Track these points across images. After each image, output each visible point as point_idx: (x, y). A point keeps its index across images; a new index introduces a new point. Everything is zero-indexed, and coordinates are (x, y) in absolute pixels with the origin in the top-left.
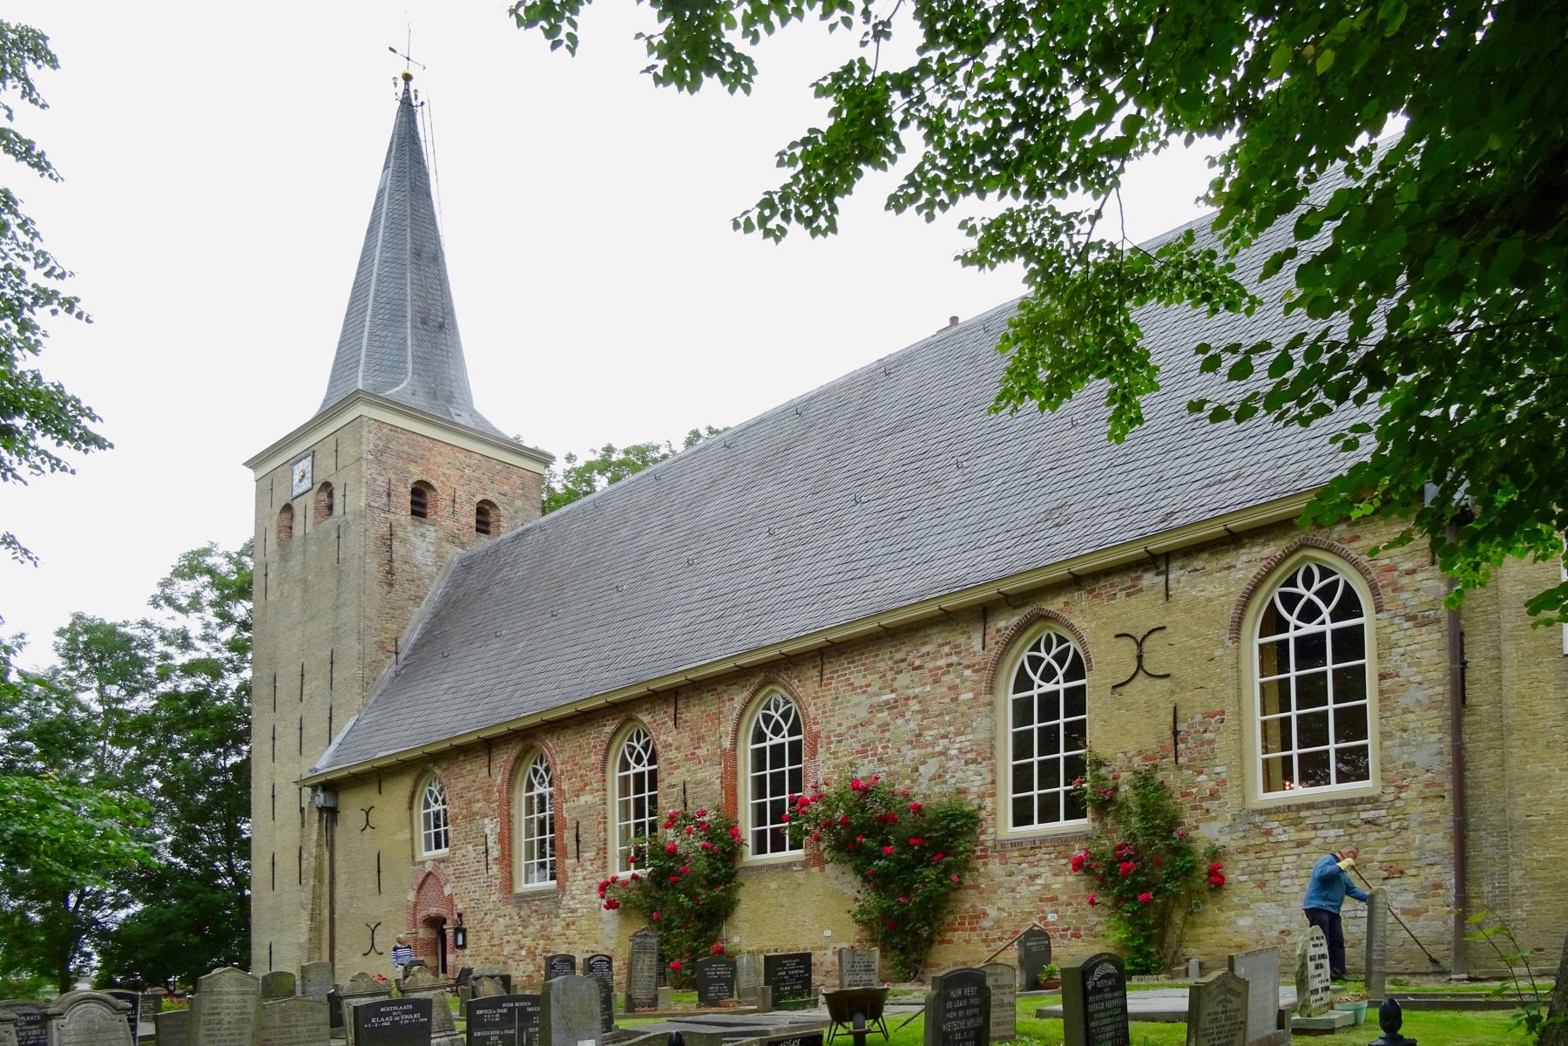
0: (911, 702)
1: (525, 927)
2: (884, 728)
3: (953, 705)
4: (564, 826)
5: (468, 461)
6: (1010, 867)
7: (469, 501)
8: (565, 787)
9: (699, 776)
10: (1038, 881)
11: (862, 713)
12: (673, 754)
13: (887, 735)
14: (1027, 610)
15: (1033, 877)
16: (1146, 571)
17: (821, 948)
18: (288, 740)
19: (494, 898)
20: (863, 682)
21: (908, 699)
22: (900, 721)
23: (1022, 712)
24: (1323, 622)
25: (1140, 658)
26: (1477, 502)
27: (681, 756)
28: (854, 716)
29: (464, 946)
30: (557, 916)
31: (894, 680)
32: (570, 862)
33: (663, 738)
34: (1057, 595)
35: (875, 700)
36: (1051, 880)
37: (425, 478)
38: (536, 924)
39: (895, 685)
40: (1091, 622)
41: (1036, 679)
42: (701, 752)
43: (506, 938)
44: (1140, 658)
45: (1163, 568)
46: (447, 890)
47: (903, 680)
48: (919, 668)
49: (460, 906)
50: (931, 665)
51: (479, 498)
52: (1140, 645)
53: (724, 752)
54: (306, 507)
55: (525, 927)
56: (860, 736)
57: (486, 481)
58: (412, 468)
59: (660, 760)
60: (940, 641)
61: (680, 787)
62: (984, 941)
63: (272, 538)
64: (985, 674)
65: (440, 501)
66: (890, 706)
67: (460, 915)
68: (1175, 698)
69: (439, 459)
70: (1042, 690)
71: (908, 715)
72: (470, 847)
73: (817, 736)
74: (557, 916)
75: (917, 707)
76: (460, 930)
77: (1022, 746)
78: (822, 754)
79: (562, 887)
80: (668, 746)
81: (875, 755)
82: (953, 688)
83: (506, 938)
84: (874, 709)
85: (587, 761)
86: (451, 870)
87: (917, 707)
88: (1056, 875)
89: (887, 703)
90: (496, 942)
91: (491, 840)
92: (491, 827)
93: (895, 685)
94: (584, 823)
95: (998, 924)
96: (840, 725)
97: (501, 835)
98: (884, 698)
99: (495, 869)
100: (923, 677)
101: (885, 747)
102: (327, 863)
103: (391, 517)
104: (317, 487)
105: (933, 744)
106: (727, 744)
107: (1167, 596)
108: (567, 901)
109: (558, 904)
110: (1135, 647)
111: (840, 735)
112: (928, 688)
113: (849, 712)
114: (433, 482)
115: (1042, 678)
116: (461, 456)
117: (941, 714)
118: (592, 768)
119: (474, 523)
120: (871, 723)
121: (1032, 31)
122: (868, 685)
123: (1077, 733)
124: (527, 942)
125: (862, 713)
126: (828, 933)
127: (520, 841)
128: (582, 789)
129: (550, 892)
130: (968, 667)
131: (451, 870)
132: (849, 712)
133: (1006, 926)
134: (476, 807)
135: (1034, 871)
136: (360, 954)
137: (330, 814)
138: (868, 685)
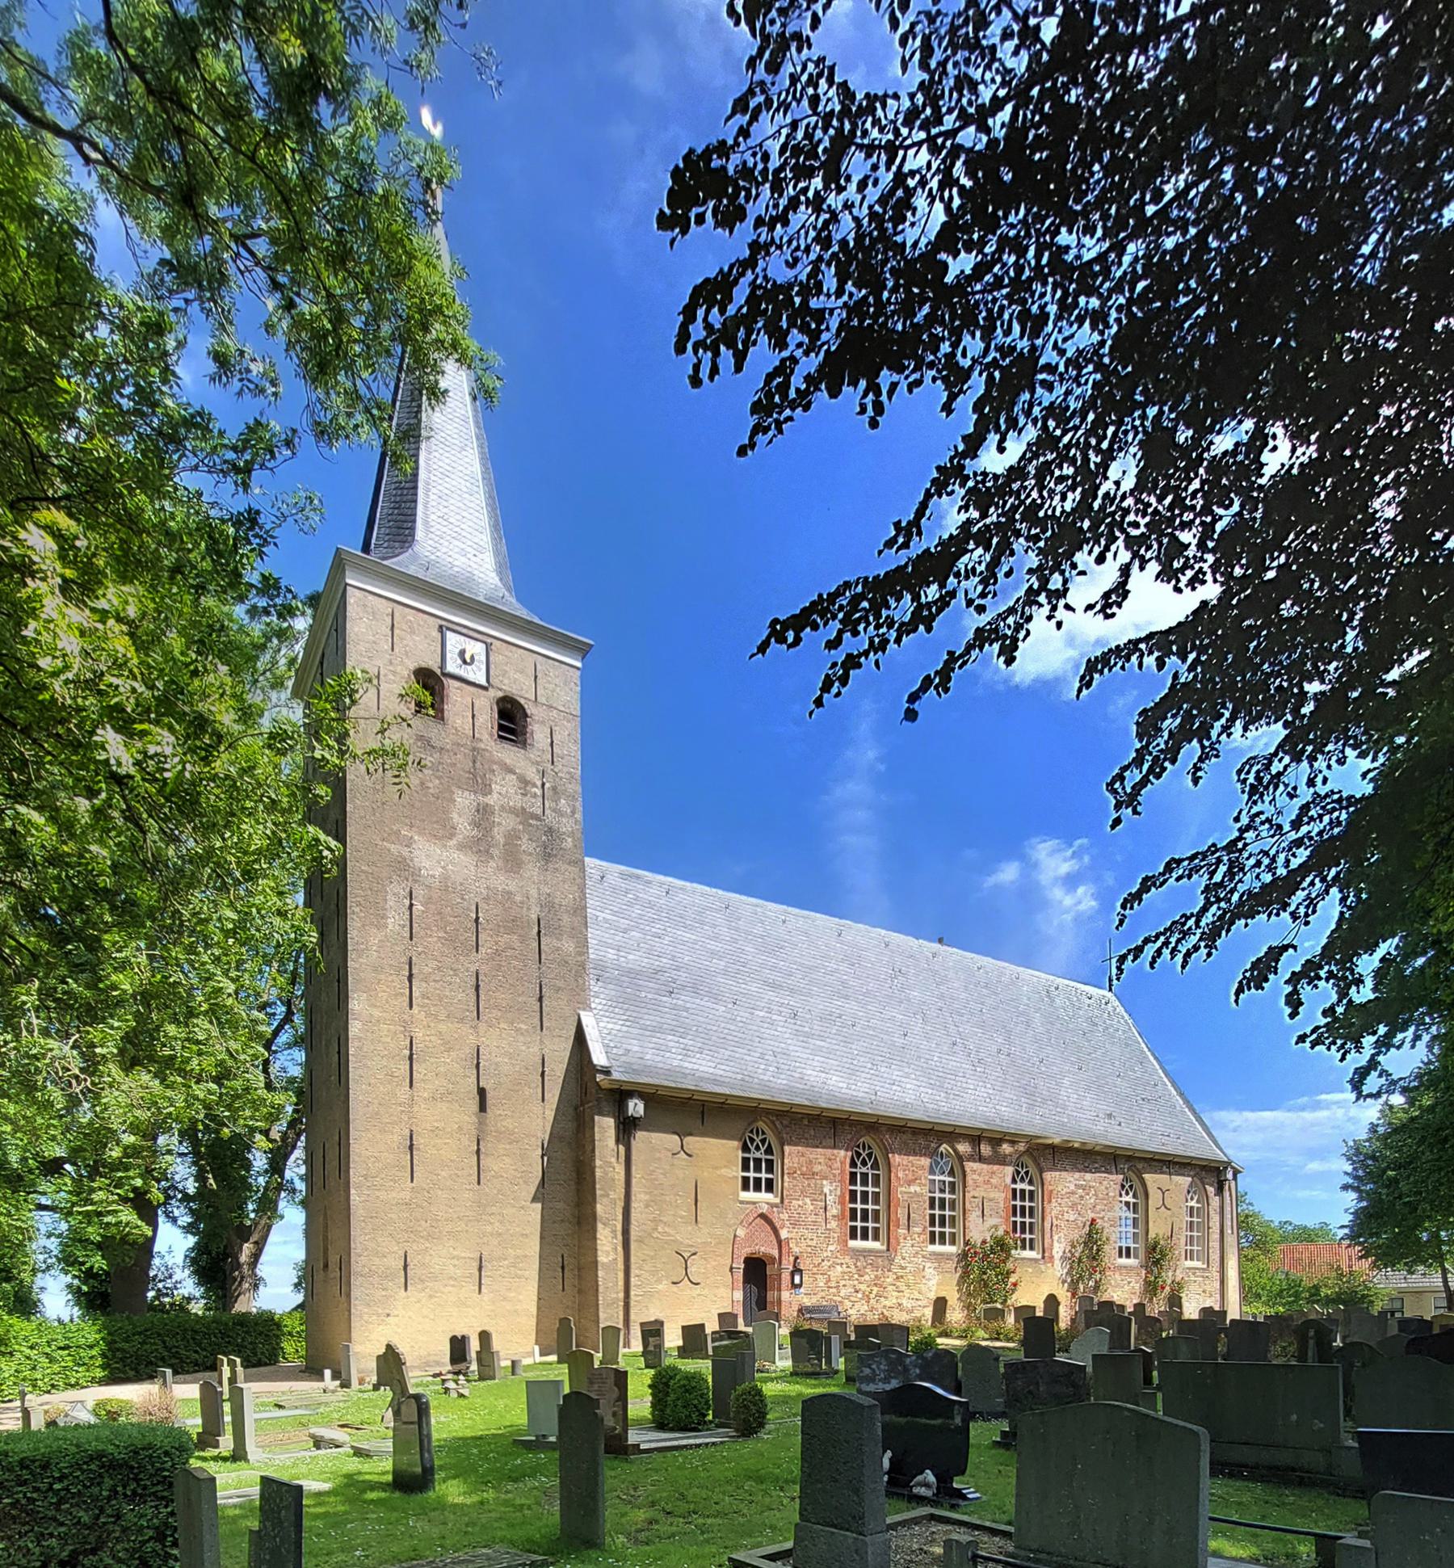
19: (831, 1248)
26: (1061, 902)
29: (800, 1286)
32: (902, 1231)
38: (870, 1275)
76: (797, 1270)
86: (785, 1216)
121: (1201, 471)
124: (863, 1287)
125: (1072, 1187)
134: (817, 1168)
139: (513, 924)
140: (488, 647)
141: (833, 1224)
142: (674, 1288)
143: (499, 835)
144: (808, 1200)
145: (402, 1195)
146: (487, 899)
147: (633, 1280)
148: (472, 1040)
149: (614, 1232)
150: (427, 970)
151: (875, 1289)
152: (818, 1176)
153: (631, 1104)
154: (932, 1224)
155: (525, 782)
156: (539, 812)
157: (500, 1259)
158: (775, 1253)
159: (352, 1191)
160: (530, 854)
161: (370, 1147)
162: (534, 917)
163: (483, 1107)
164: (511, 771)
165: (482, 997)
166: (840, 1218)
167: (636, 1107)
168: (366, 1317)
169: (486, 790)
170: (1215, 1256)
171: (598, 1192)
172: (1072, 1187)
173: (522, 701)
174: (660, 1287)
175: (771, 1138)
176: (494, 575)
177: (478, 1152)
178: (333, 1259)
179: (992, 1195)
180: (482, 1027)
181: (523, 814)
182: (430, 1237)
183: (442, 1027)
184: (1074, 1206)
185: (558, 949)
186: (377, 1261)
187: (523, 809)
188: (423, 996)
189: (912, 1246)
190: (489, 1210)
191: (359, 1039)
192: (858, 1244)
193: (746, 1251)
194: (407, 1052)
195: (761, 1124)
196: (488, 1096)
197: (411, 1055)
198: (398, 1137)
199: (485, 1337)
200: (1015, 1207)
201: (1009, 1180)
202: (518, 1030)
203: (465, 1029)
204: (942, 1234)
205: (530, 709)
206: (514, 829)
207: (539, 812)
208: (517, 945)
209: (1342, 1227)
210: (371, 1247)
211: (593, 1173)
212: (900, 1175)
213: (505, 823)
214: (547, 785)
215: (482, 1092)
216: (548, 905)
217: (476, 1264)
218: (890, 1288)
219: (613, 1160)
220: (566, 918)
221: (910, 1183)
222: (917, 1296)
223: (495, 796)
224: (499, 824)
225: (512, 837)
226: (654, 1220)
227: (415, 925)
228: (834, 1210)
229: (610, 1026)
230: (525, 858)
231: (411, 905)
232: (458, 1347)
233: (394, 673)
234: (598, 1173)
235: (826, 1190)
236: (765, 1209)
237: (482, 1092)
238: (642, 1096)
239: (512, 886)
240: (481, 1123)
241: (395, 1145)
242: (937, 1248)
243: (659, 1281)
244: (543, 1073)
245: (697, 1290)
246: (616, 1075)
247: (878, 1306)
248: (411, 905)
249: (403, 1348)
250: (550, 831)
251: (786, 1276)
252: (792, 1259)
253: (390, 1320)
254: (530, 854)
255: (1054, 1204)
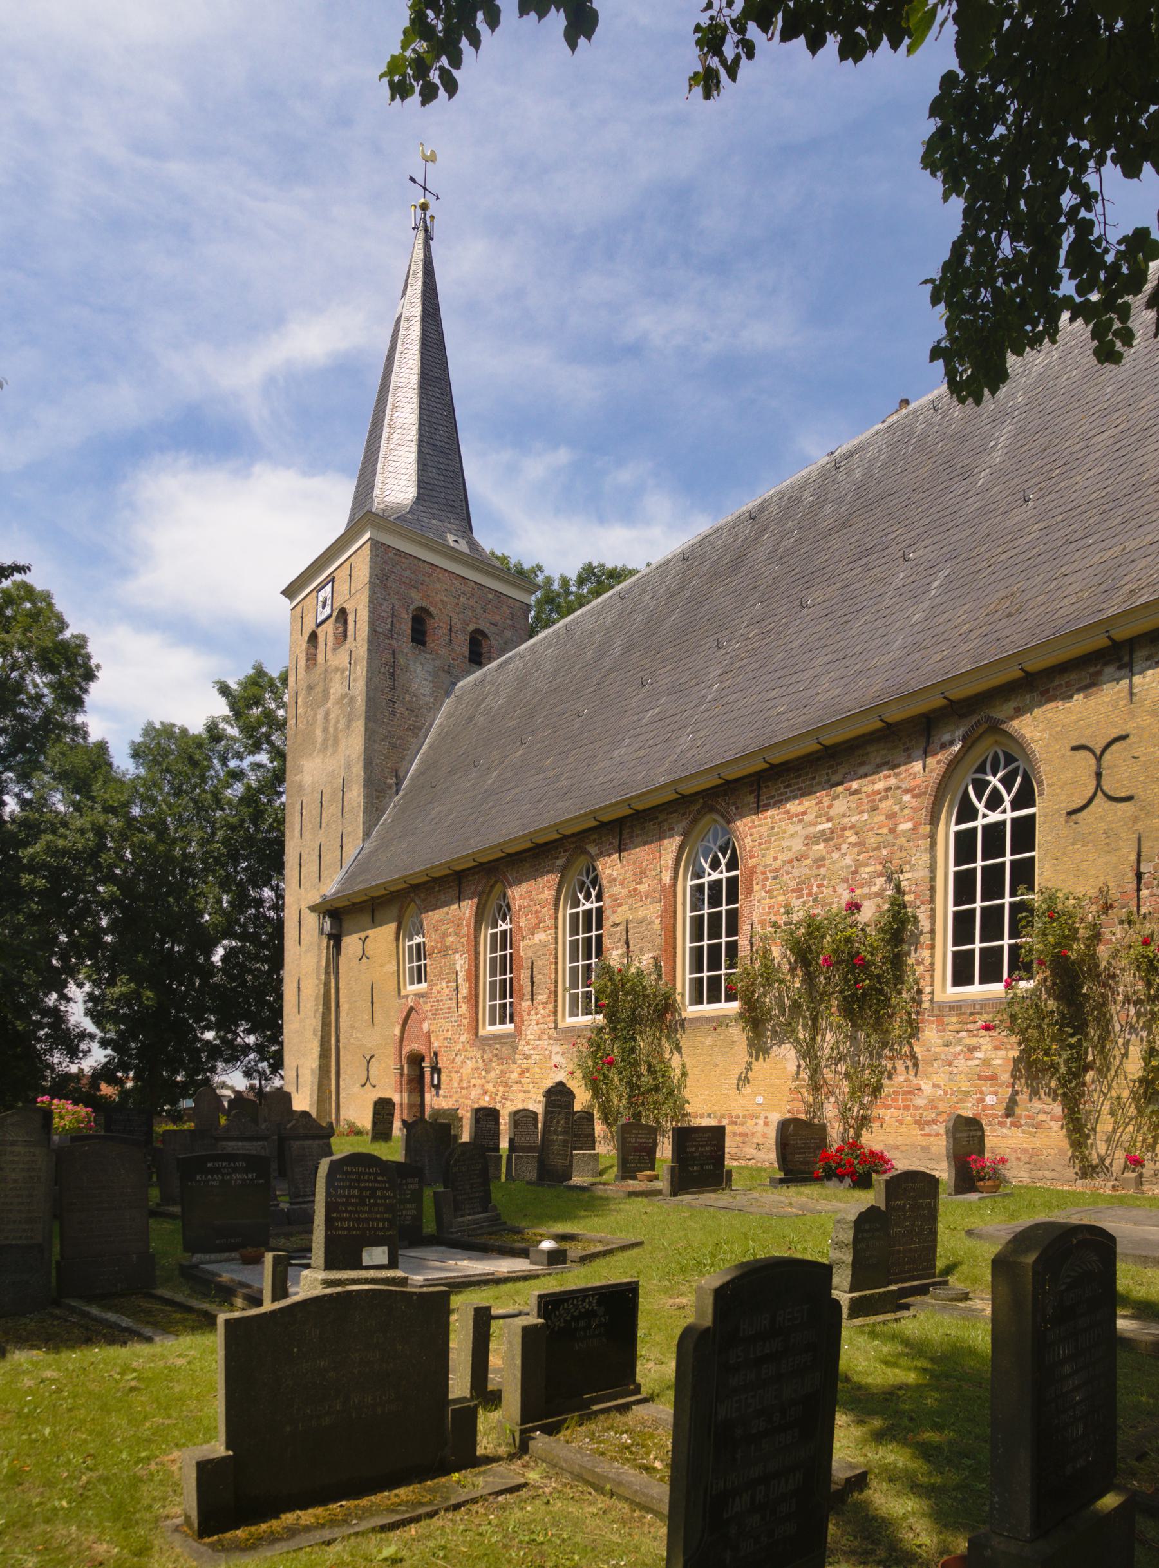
0: (848, 833)
1: (488, 1072)
2: (820, 862)
3: (891, 837)
4: (521, 966)
5: (463, 588)
6: (948, 1035)
7: (464, 630)
8: (522, 924)
9: (641, 914)
10: (978, 1055)
11: (797, 845)
12: (617, 890)
13: (823, 871)
14: (974, 719)
15: (972, 1049)
16: (1106, 664)
17: (753, 1117)
18: (310, 868)
19: (463, 1038)
20: (800, 809)
21: (844, 829)
22: (836, 855)
23: (965, 847)
24: (1004, 811)
25: (1099, 775)
27: (624, 891)
28: (789, 849)
30: (514, 1062)
31: (830, 806)
32: (526, 1004)
33: (608, 871)
34: (1007, 700)
35: (811, 829)
36: (991, 1054)
37: (424, 604)
39: (832, 813)
40: (1040, 729)
41: (981, 807)
42: (643, 888)
43: (473, 1081)
44: (1099, 775)
45: (1126, 659)
46: (425, 1027)
47: (840, 806)
48: (857, 792)
49: (436, 1045)
50: (868, 789)
51: (471, 628)
52: (1099, 759)
53: (664, 887)
54: (328, 632)
55: (488, 1072)
56: (796, 873)
57: (479, 611)
58: (414, 594)
59: (606, 896)
60: (879, 760)
61: (623, 927)
62: (917, 1122)
63: (302, 663)
64: (927, 801)
65: (437, 628)
66: (825, 837)
67: (436, 1054)
68: (1140, 826)
69: (438, 586)
70: (987, 821)
71: (844, 847)
72: (444, 984)
73: (752, 871)
74: (514, 1062)
75: (853, 839)
76: (436, 1069)
77: (964, 887)
78: (758, 893)
79: (518, 1030)
80: (612, 881)
81: (809, 894)
82: (892, 816)
83: (473, 1081)
84: (810, 841)
85: (541, 896)
86: (428, 1007)
87: (853, 839)
88: (996, 1048)
89: (823, 832)
90: (465, 1084)
91: (461, 976)
92: (461, 963)
93: (832, 813)
94: (538, 963)
95: (933, 1102)
96: (775, 859)
97: (468, 971)
98: (820, 827)
99: (464, 1008)
100: (860, 802)
101: (820, 886)
102: (333, 991)
103: (394, 642)
104: (335, 613)
105: (870, 883)
106: (667, 878)
107: (1131, 694)
108: (522, 1047)
109: (515, 1048)
110: (1093, 761)
111: (776, 870)
112: (865, 816)
113: (785, 844)
114: (432, 609)
115: (987, 806)
116: (457, 583)
117: (878, 848)
118: (544, 904)
119: (467, 654)
120: (806, 857)
122: (804, 813)
123: (1024, 873)
125: (797, 845)
126: (760, 1100)
127: (485, 979)
128: (537, 926)
129: (509, 1036)
130: (907, 791)
131: (428, 1007)
132: (785, 844)
133: (942, 1106)
135: (973, 1041)
136: (358, 1085)
137: (336, 939)
138: (804, 813)
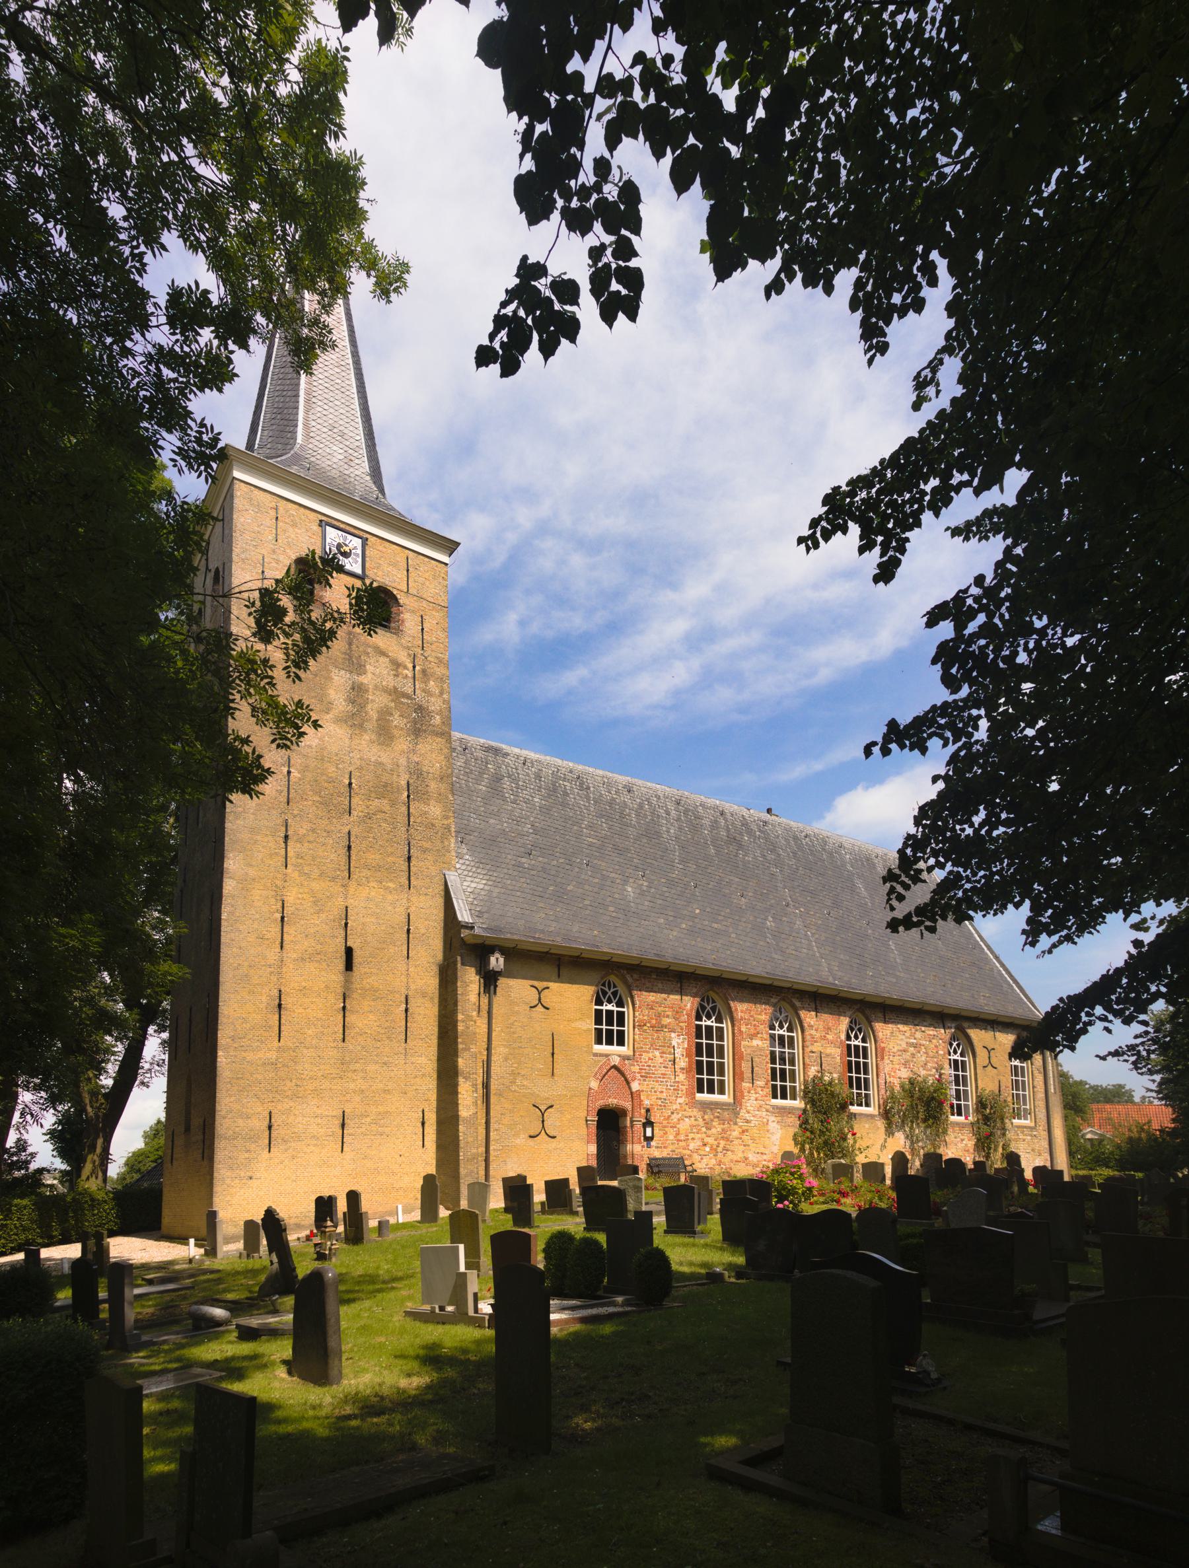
19: (680, 1100)
29: (652, 1138)
32: (746, 1085)
38: (717, 1127)
76: (649, 1123)
86: (636, 1069)
124: (710, 1140)
139: (384, 790)
140: (365, 542)
141: (682, 1077)
142: (531, 1142)
143: (372, 711)
144: (657, 1053)
145: (268, 1055)
146: (360, 769)
147: (492, 1134)
148: (340, 902)
149: (475, 1085)
150: (302, 831)
151: (722, 1143)
152: (662, 1027)
153: (493, 960)
154: (774, 1078)
155: (396, 665)
156: (410, 691)
157: (362, 1116)
158: (630, 1108)
159: (220, 1053)
160: (402, 729)
161: (239, 1008)
162: (403, 783)
163: (349, 966)
164: (383, 654)
165: (353, 857)
166: (687, 1071)
167: (496, 962)
168: (228, 1181)
169: (360, 669)
170: (1042, 1115)
171: (460, 1046)
172: (904, 1046)
173: (395, 592)
174: (518, 1141)
175: (622, 990)
176: (368, 478)
177: (344, 1008)
178: (196, 1122)
179: (829, 1051)
180: (353, 885)
181: (396, 694)
182: (295, 1096)
183: (315, 885)
184: (905, 1065)
185: (426, 813)
186: (240, 1122)
187: (395, 688)
188: (299, 856)
189: (757, 1101)
190: (352, 1067)
191: (233, 897)
192: (705, 1097)
193: (600, 1103)
194: (279, 916)
195: (613, 978)
196: (355, 954)
197: (283, 918)
198: (265, 998)
199: (353, 1198)
200: (850, 1062)
201: (843, 1037)
202: (387, 888)
203: (337, 888)
204: (784, 1088)
205: (402, 598)
206: (386, 706)
207: (410, 691)
208: (387, 808)
209: (522, 156)
210: (235, 1109)
211: (455, 1026)
212: (743, 1029)
213: (377, 702)
214: (417, 668)
215: (349, 952)
216: (417, 772)
217: (338, 1122)
218: (736, 1142)
219: (475, 1013)
220: (433, 785)
221: (752, 1037)
222: (762, 1150)
223: (370, 675)
224: (373, 701)
225: (384, 714)
226: (513, 1073)
227: (292, 791)
228: (682, 1063)
229: (473, 885)
230: (395, 732)
231: (289, 772)
232: (324, 1206)
233: (278, 561)
234: (461, 1027)
235: (674, 1043)
236: (616, 1061)
237: (349, 952)
238: (505, 951)
239: (385, 758)
240: (347, 982)
241: (263, 1006)
242: (779, 1102)
243: (516, 1135)
244: (408, 931)
245: (554, 1144)
246: (477, 931)
247: (726, 1160)
248: (289, 772)
249: (282, 1213)
250: (420, 709)
251: (638, 1126)
252: (643, 1111)
253: (254, 1183)
254: (402, 729)
255: (886, 1061)
